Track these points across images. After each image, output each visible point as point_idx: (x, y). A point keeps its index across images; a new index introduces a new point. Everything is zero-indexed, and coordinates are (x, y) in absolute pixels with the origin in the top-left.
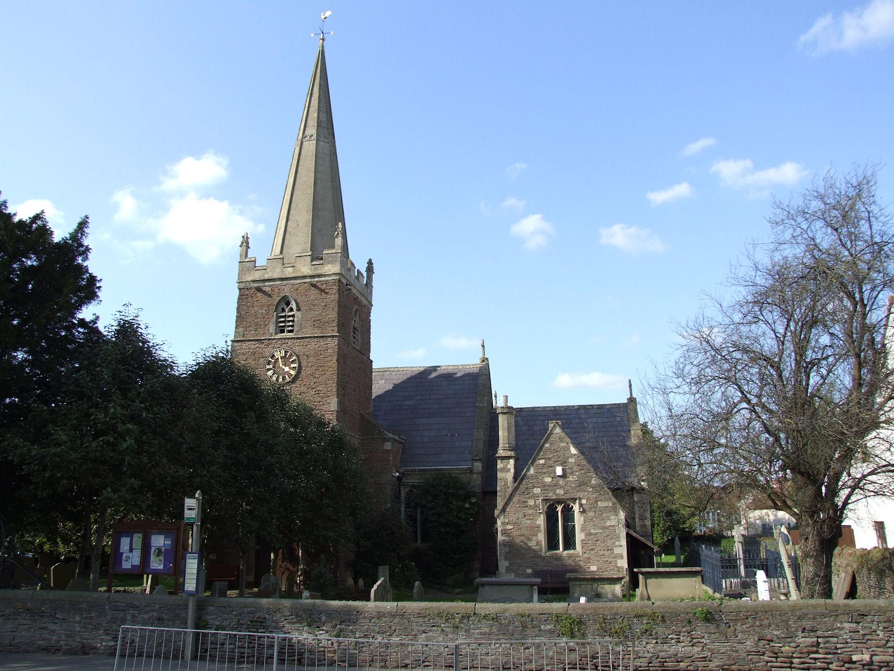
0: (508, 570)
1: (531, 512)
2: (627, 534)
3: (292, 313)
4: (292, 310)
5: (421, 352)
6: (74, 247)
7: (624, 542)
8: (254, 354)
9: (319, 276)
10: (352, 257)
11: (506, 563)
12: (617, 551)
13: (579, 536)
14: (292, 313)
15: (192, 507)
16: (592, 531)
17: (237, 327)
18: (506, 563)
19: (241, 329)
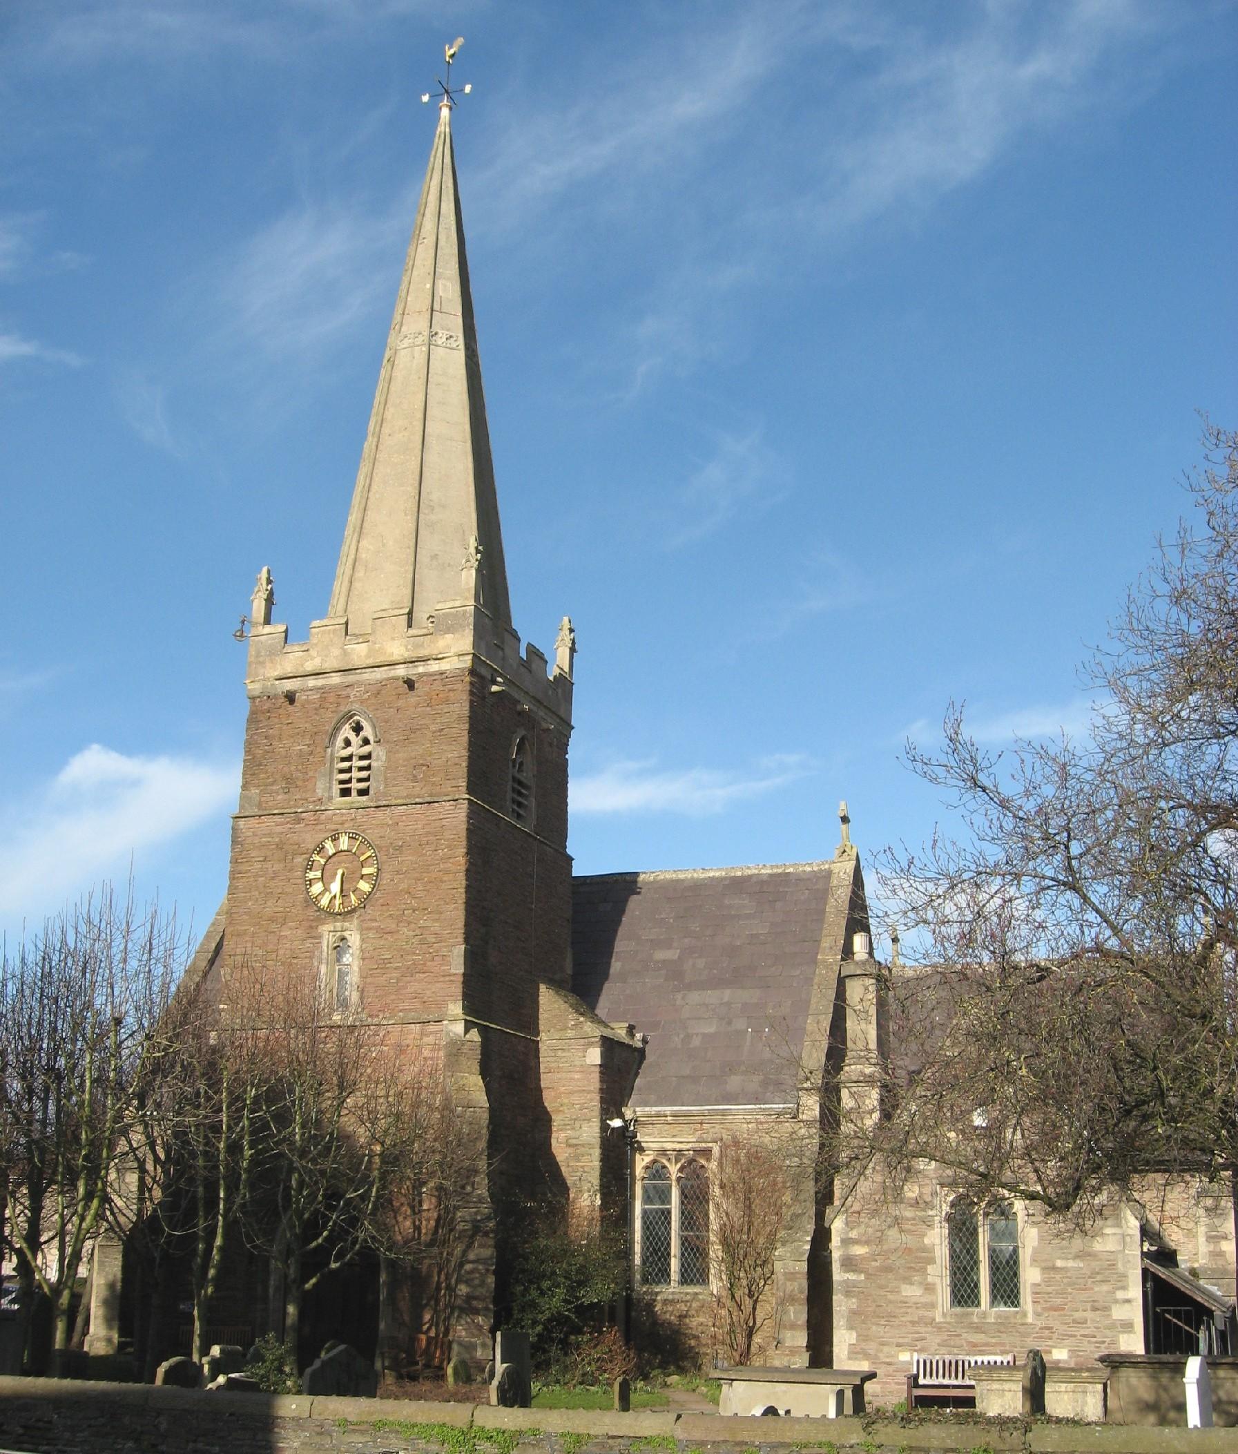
0: (854, 1353)
1: (909, 1213)
2: (1145, 1271)
3: (366, 749)
4: (366, 742)
5: (331, 1407)
6: (564, 685)
7: (1135, 1291)
8: (280, 846)
9: (425, 660)
10: (520, 621)
11: (852, 1337)
12: (1118, 1313)
13: (1029, 1275)
14: (366, 749)
15: (16, 1307)
16: (1059, 1263)
17: (245, 787)
18: (852, 1337)
19: (254, 791)
